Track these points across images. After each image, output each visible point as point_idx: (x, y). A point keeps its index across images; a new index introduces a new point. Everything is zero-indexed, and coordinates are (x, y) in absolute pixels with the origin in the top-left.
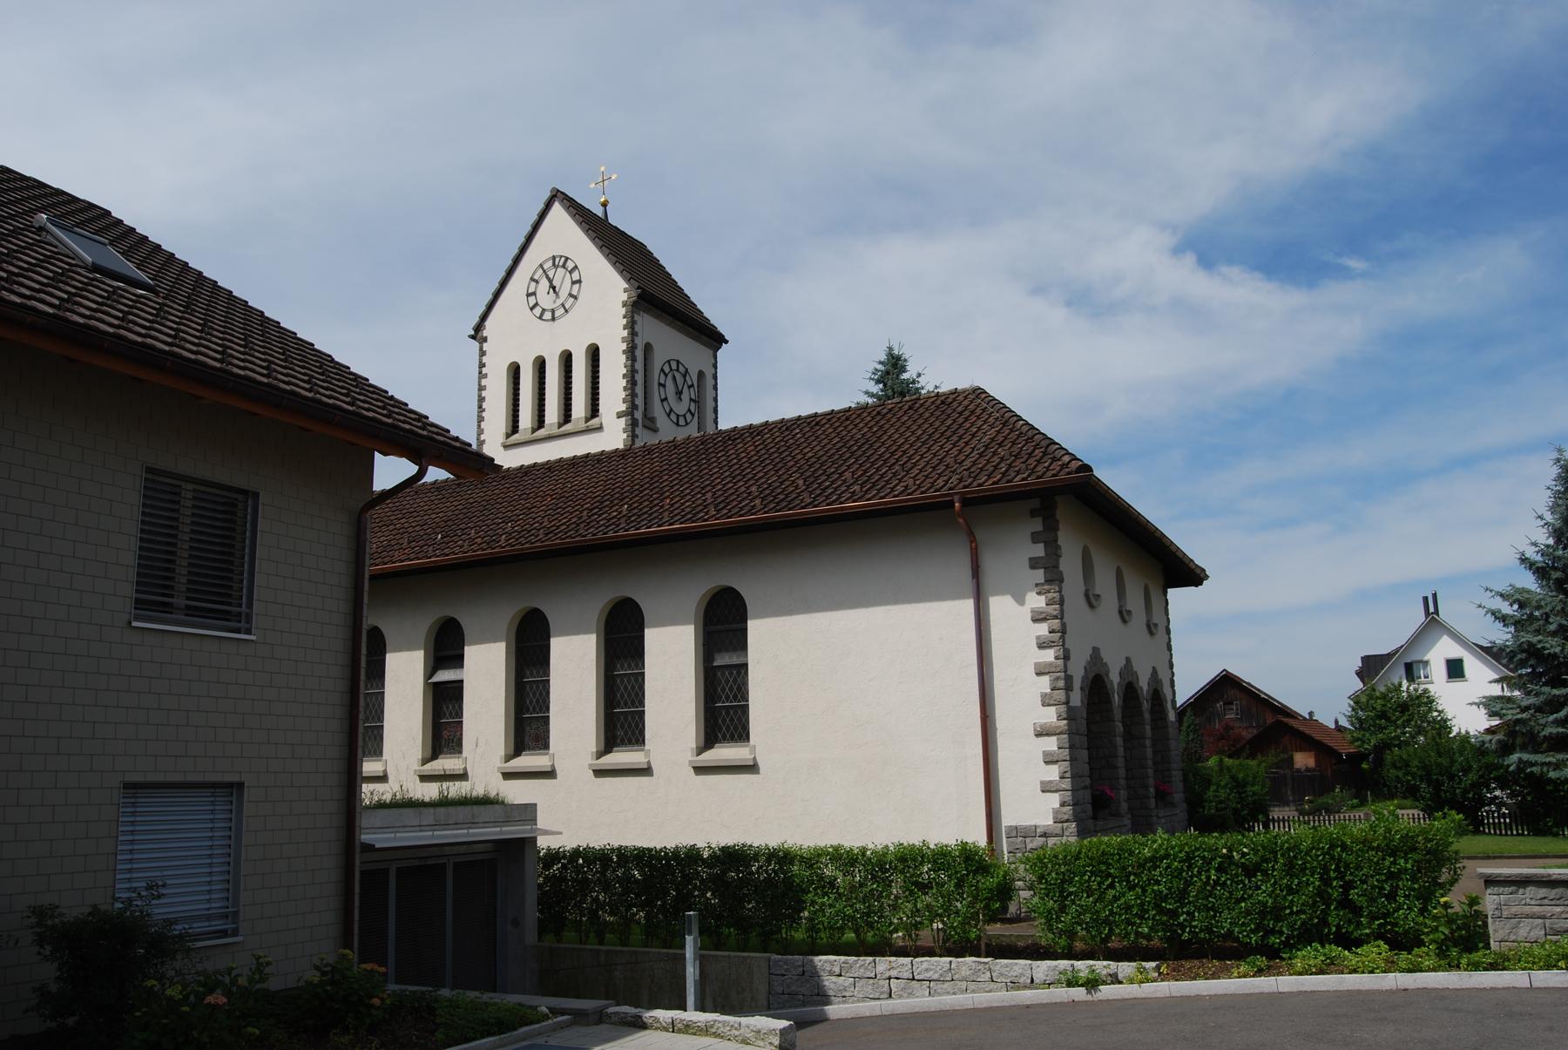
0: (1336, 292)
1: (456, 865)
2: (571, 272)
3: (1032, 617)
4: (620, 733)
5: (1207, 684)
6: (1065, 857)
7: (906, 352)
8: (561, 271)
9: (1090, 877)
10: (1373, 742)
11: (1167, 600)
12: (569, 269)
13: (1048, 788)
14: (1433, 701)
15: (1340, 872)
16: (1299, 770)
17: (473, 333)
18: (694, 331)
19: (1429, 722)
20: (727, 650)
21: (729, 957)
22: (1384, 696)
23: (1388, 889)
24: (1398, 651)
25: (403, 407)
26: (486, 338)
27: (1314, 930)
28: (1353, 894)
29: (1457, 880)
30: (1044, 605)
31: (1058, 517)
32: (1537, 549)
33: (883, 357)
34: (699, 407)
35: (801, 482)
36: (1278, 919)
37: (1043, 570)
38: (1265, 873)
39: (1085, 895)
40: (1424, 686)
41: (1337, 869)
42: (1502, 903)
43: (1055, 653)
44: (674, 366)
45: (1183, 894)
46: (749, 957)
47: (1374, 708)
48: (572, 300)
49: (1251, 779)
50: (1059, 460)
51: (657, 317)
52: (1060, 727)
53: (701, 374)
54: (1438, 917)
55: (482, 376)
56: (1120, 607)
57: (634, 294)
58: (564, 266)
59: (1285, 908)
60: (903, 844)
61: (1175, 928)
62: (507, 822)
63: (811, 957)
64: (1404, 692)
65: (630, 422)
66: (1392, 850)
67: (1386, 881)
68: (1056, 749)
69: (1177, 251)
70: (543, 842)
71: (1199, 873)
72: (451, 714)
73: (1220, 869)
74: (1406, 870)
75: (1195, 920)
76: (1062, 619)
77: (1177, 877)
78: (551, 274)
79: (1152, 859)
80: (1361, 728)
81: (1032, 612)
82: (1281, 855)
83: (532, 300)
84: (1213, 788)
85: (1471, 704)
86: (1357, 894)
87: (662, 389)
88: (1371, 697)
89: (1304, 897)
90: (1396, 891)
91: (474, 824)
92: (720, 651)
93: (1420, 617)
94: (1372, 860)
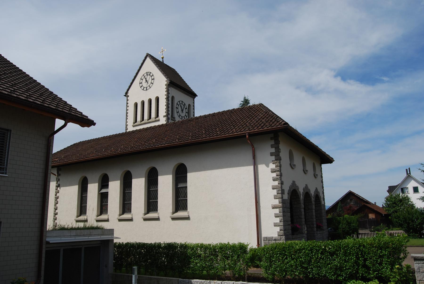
0: (380, 87)
1: (64, 250)
2: (151, 77)
3: (271, 171)
4: (152, 208)
5: (345, 195)
6: (272, 248)
7: (249, 98)
8: (149, 76)
9: (279, 255)
10: (392, 211)
11: (321, 168)
12: (151, 76)
13: (276, 225)
14: (409, 199)
15: (363, 255)
16: (370, 219)
17: (125, 94)
18: (187, 93)
19: (408, 205)
20: (182, 182)
21: (166, 279)
22: (395, 198)
23: (379, 261)
24: (399, 185)
26: (129, 96)
27: (354, 275)
28: (367, 263)
29: (406, 257)
30: (275, 167)
31: (279, 140)
33: (243, 100)
34: (188, 115)
35: (204, 131)
36: (341, 271)
37: (274, 156)
38: (337, 255)
39: (278, 261)
40: (406, 195)
41: (361, 254)
42: (420, 267)
43: (278, 182)
44: (181, 102)
45: (310, 261)
46: (172, 279)
47: (392, 201)
48: (152, 84)
49: (352, 222)
50: (279, 122)
51: (176, 89)
52: (280, 206)
53: (189, 105)
54: (396, 272)
55: (127, 106)
56: (304, 169)
57: (168, 82)
58: (150, 75)
59: (344, 267)
60: (222, 243)
61: (307, 273)
62: (103, 235)
63: (191, 280)
64: (400, 196)
65: (167, 118)
66: (380, 247)
67: (378, 258)
68: (279, 212)
69: (336, 76)
70: (115, 241)
71: (315, 255)
72: (105, 202)
73: (322, 253)
74: (386, 255)
75: (314, 271)
76: (280, 171)
77: (307, 256)
78: (146, 77)
79: (299, 250)
80: (388, 207)
81: (271, 169)
82: (342, 249)
83: (141, 85)
84: (341, 224)
85: (418, 199)
86: (369, 263)
87: (177, 109)
88: (391, 198)
89: (350, 263)
90: (382, 262)
91: (90, 235)
92: (180, 183)
93: (405, 175)
94: (373, 251)
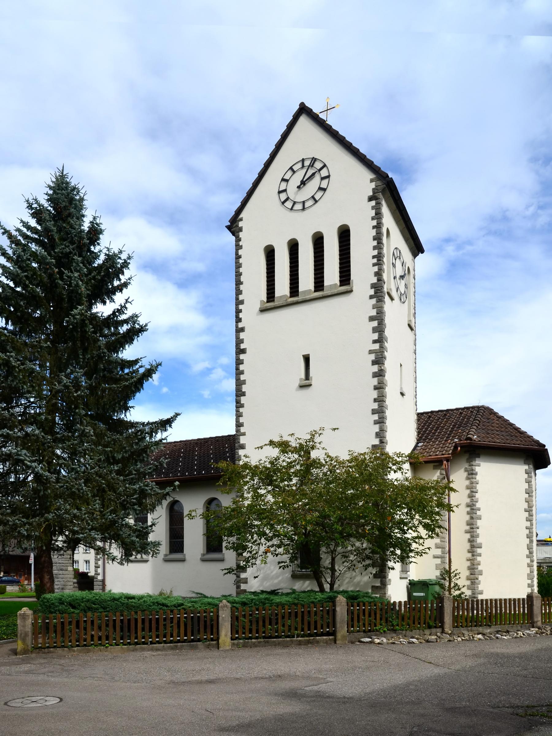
25: (436, 464)
32: (107, 253)
